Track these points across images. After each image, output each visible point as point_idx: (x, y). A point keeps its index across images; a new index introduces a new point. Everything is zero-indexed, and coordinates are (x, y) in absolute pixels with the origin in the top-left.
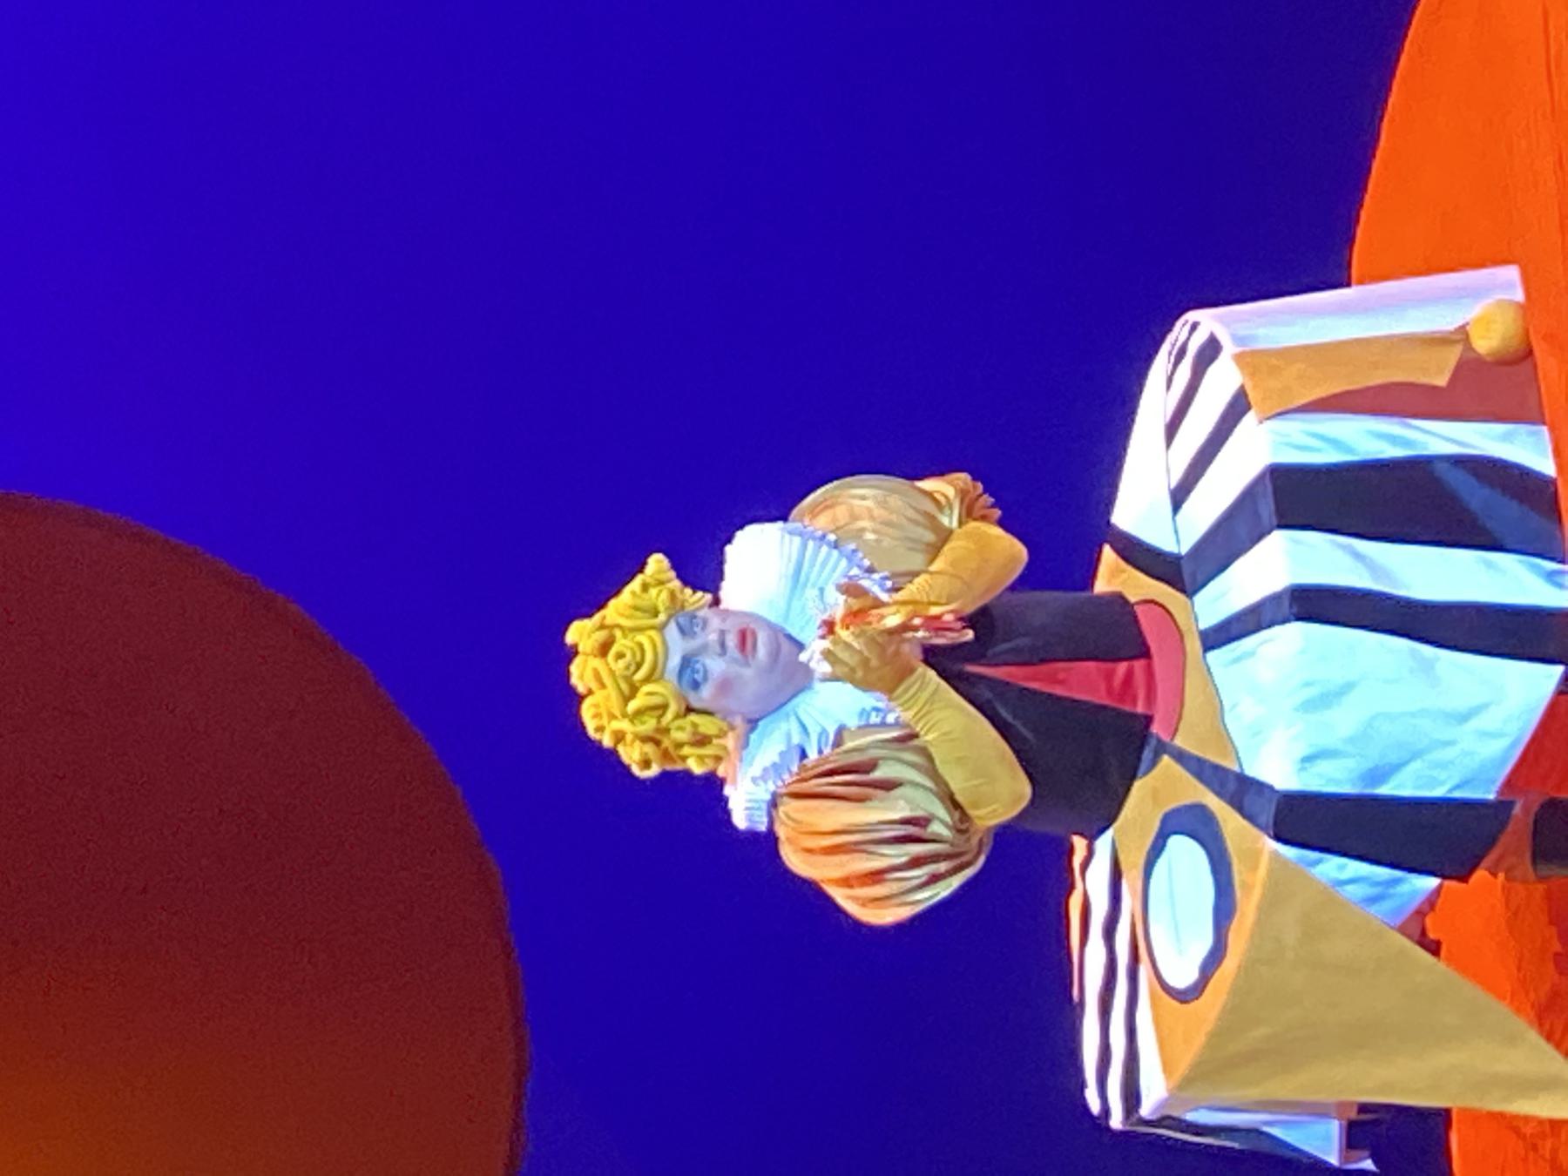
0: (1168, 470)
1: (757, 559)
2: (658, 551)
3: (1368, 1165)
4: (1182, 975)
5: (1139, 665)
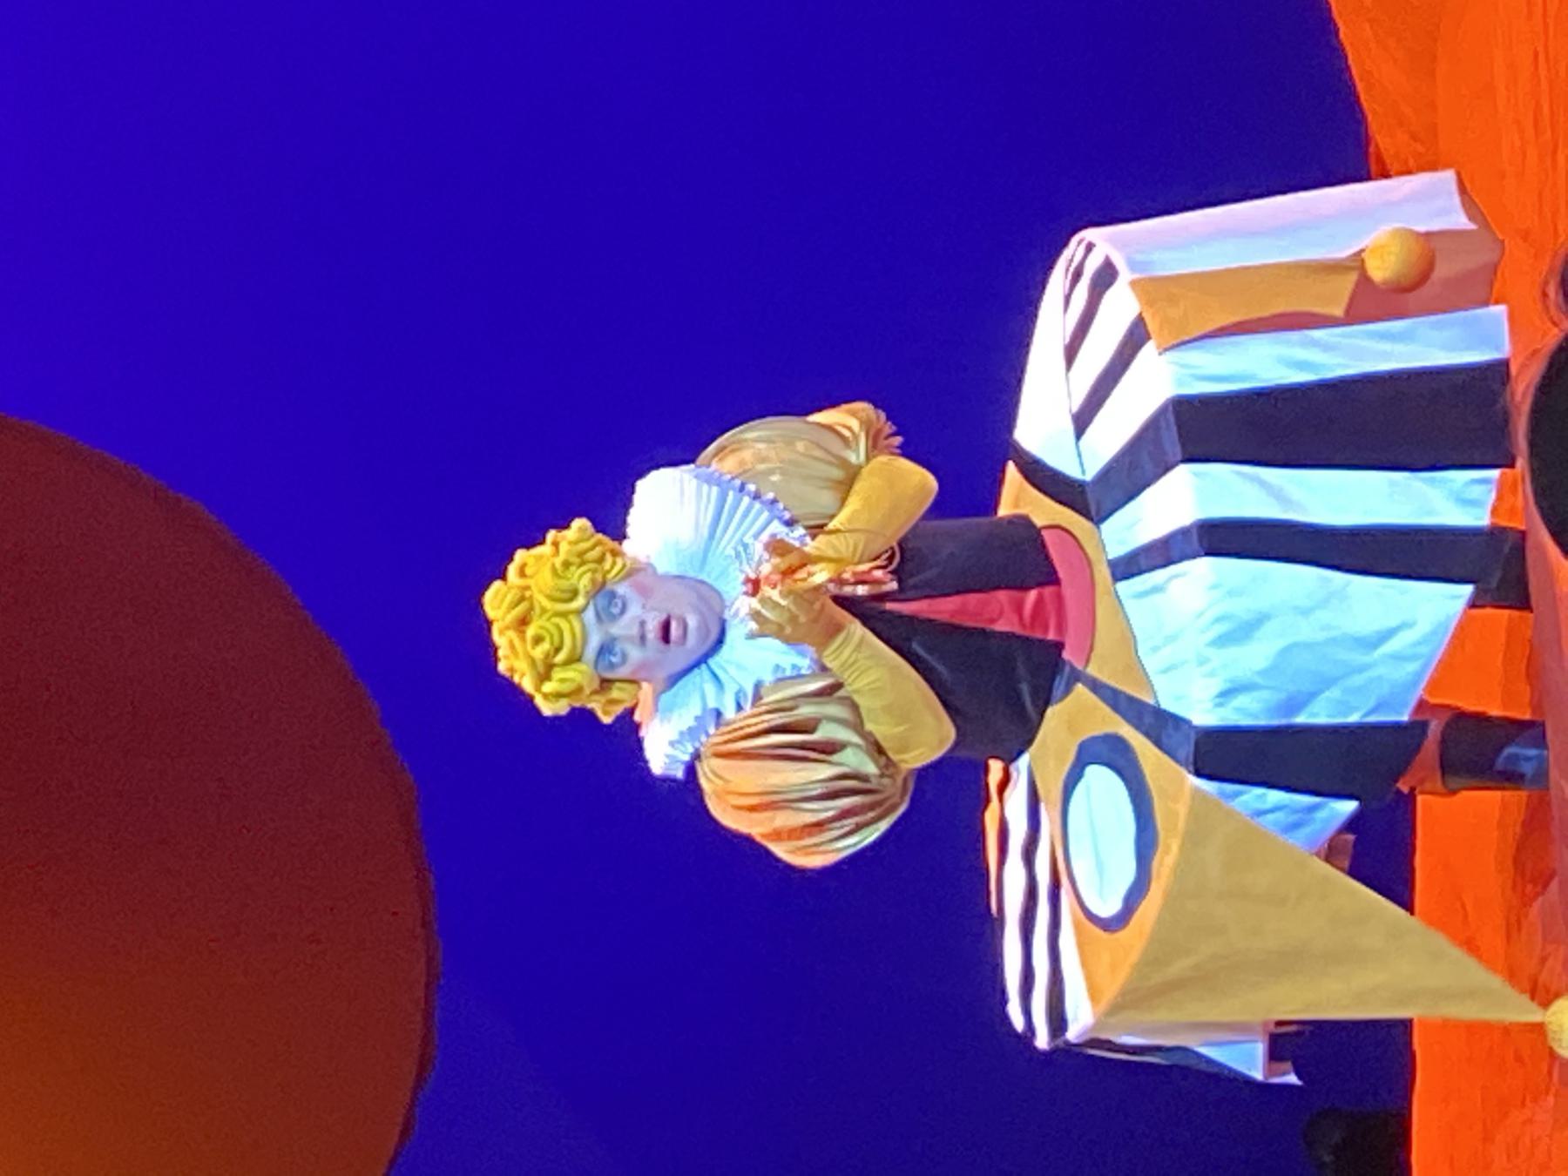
0: (1069, 395)
1: (668, 508)
2: (580, 515)
3: (1292, 1079)
4: (1107, 906)
5: (1048, 591)
